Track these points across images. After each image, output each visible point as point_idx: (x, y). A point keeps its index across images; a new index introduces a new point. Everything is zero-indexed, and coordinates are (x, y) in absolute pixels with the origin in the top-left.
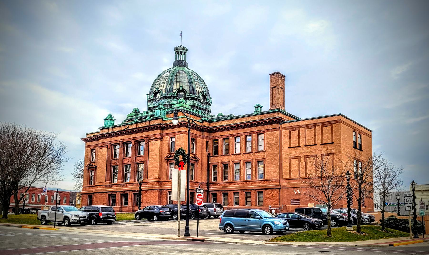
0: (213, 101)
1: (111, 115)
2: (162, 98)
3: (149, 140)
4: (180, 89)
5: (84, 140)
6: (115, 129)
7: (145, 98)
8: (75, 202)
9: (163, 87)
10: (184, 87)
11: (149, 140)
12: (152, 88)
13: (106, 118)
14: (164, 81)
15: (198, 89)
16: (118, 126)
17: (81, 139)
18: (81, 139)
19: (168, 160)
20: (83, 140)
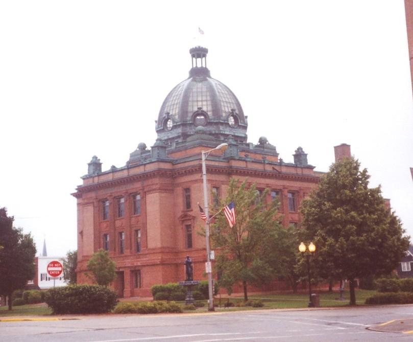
0: (249, 121)
1: (97, 158)
2: (174, 127)
3: (145, 192)
4: (197, 111)
5: (74, 196)
6: (116, 175)
7: (153, 126)
8: (353, 223)
9: (175, 111)
10: (205, 109)
11: (145, 192)
12: (161, 114)
13: (89, 162)
14: (176, 102)
15: (226, 108)
16: (106, 173)
17: (71, 194)
18: (71, 194)
19: (183, 221)
20: (74, 195)
